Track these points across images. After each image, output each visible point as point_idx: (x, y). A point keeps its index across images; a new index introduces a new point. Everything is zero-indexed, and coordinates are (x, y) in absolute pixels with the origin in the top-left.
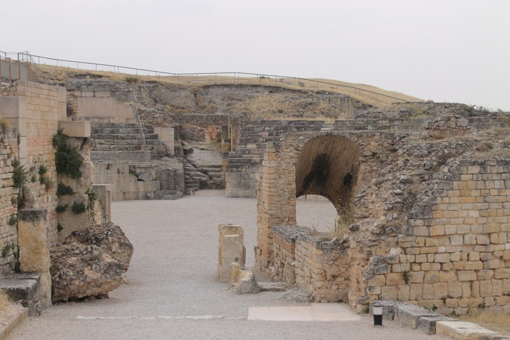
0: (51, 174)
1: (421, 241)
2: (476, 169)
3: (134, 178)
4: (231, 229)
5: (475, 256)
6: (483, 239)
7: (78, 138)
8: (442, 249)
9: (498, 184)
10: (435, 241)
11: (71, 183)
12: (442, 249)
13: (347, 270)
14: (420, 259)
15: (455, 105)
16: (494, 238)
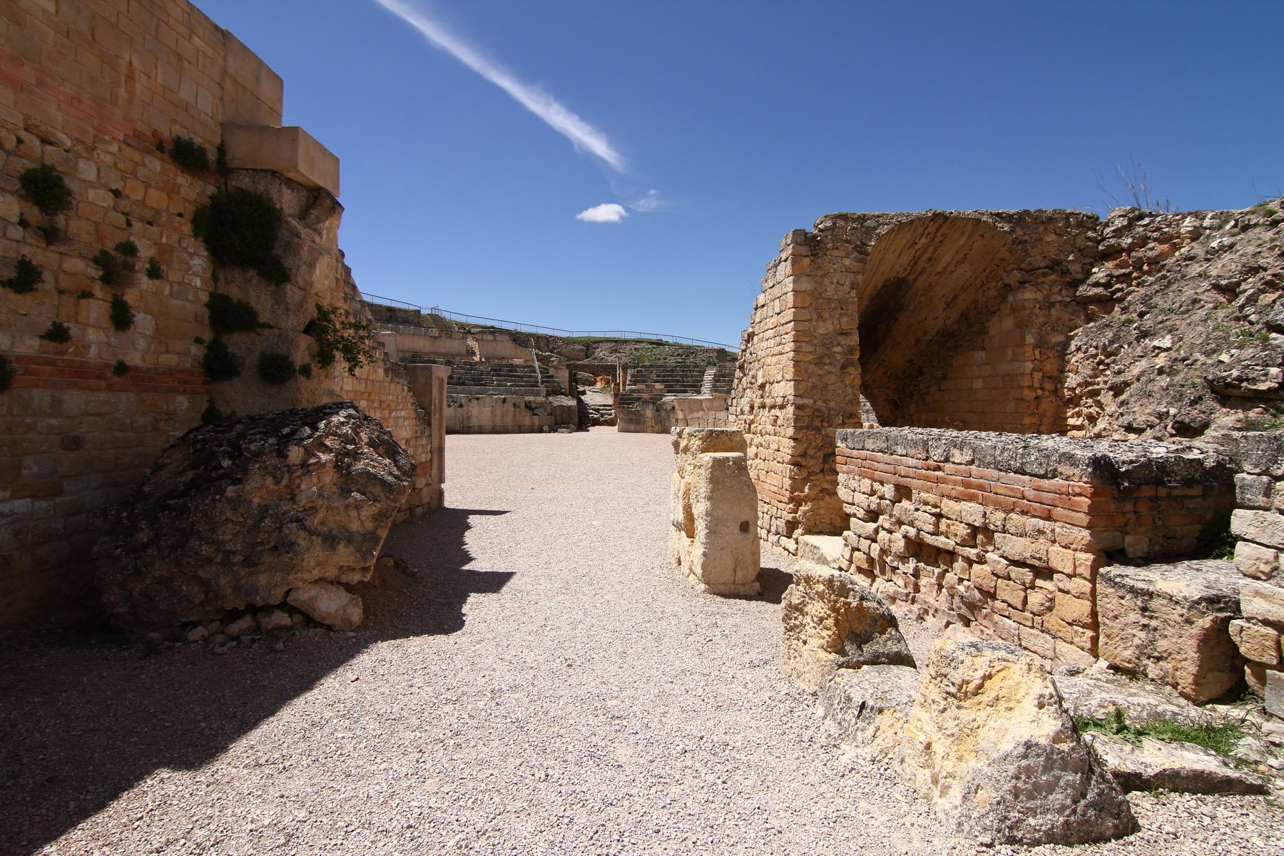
3: (529, 413)
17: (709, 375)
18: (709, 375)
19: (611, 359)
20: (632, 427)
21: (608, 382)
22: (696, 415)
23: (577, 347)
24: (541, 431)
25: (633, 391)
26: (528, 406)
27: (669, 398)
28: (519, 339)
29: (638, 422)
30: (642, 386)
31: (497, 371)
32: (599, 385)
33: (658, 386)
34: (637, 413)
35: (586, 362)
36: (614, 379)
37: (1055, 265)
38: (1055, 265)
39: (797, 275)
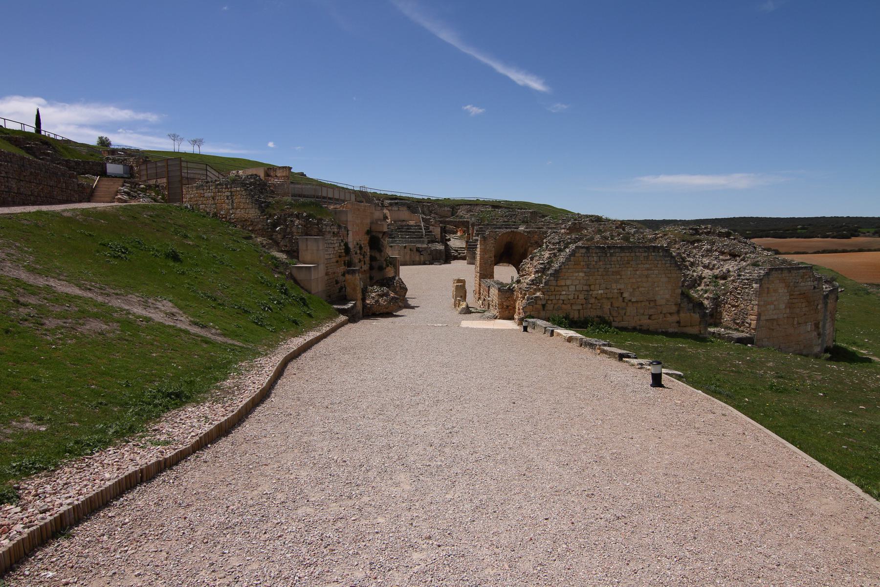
0: (367, 249)
1: (552, 288)
2: (584, 251)
3: (418, 254)
4: (459, 281)
5: (581, 296)
6: (585, 288)
7: (380, 232)
8: (564, 293)
9: (595, 259)
10: (560, 289)
11: (377, 255)
12: (564, 293)
13: (588, 266)
14: (552, 297)
15: (592, 216)
16: (592, 287)
21: (464, 232)
24: (425, 264)
26: (418, 250)
31: (400, 228)
32: (459, 234)
35: (451, 219)
37: (536, 242)
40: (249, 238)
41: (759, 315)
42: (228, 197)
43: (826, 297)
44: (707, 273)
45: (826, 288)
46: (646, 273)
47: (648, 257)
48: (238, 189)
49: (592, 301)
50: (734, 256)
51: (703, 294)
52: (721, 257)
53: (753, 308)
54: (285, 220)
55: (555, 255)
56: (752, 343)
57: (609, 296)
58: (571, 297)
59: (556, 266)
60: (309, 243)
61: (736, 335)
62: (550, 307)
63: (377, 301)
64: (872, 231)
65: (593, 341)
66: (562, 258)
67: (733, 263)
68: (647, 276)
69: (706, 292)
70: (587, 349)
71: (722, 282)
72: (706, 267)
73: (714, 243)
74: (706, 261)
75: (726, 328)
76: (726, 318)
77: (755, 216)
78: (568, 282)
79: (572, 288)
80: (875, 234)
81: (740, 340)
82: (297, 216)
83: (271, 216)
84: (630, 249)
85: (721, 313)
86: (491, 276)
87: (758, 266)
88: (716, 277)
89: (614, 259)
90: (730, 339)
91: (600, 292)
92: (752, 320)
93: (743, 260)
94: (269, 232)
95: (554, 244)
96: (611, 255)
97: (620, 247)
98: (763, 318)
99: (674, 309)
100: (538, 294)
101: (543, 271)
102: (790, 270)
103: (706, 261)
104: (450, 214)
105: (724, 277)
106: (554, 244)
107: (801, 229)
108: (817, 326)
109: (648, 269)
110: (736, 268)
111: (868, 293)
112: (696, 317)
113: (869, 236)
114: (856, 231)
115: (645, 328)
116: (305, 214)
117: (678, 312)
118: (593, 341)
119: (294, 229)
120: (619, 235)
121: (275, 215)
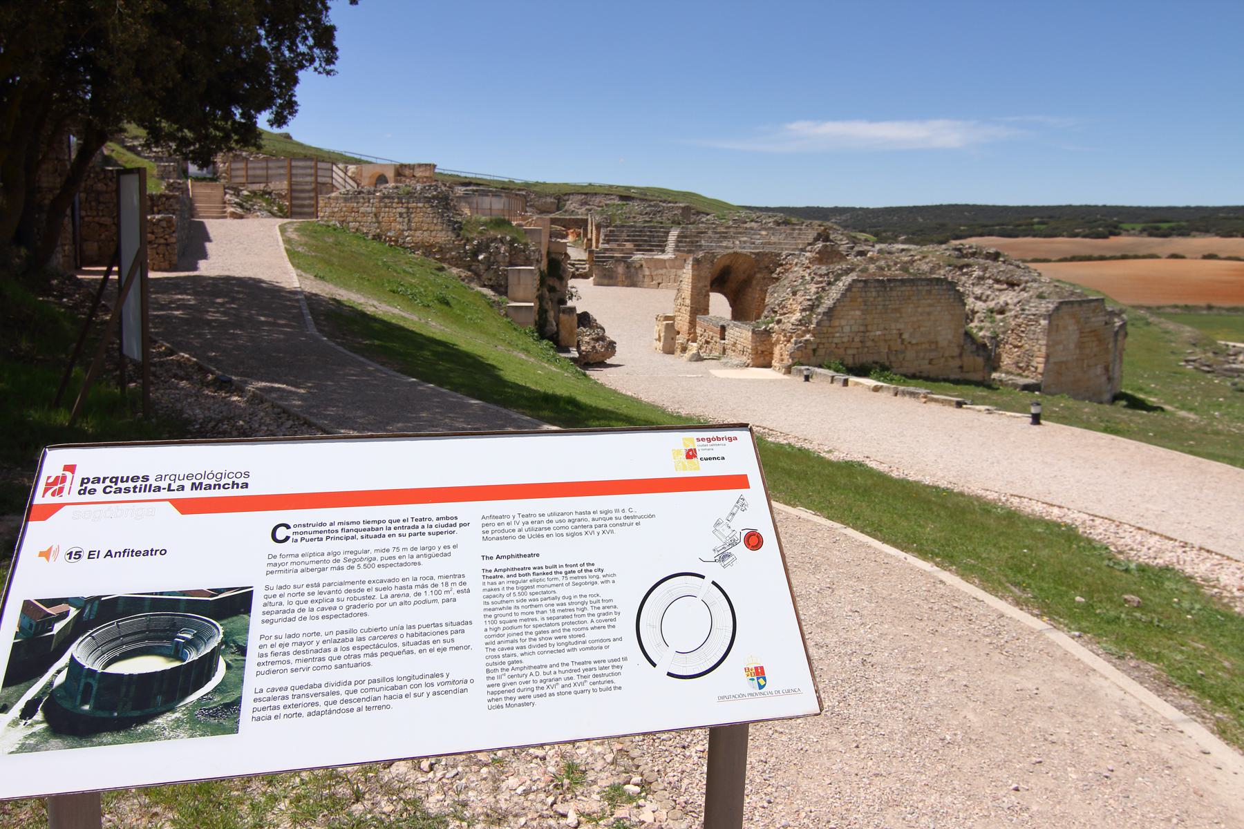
2: (861, 285)
5: (857, 339)
17: (674, 234)
18: (674, 234)
19: (581, 213)
20: (606, 281)
21: (578, 235)
22: (660, 272)
23: (549, 200)
25: (606, 250)
27: (638, 256)
28: (626, 196)
29: (611, 277)
30: (613, 245)
33: (629, 245)
34: (610, 270)
36: (585, 235)
37: (767, 267)
38: (767, 267)
39: (693, 269)
40: (441, 269)
41: (1047, 357)
42: (401, 215)
43: (1116, 333)
44: (979, 305)
45: (1118, 323)
46: (928, 309)
47: (929, 292)
48: (420, 205)
49: (869, 344)
50: (1012, 285)
51: (981, 330)
52: (996, 286)
53: (1039, 349)
54: (488, 247)
55: (823, 289)
56: (1039, 390)
57: (888, 337)
58: (845, 340)
59: (828, 303)
60: (522, 275)
61: (1022, 381)
62: (821, 352)
63: (594, 347)
64: (1139, 227)
65: (912, 389)
66: (835, 293)
67: (1012, 293)
68: (929, 314)
69: (981, 329)
70: (907, 398)
71: (999, 317)
72: (978, 298)
73: (986, 269)
74: (978, 291)
75: (1008, 373)
76: (1006, 361)
77: (971, 203)
78: (843, 322)
79: (847, 329)
80: (1142, 231)
81: (1026, 387)
82: (502, 241)
83: (468, 240)
84: (913, 282)
85: (1000, 355)
86: (705, 311)
87: (1044, 298)
88: (991, 311)
89: (894, 293)
90: (1015, 386)
91: (878, 333)
92: (1039, 363)
93: (1024, 290)
94: (467, 261)
95: (821, 276)
96: (891, 289)
97: (902, 280)
98: (1052, 360)
99: (956, 351)
100: (808, 336)
101: (812, 308)
102: (1081, 303)
103: (978, 291)
104: (554, 207)
105: (1002, 312)
106: (821, 276)
107: (1039, 223)
108: (1107, 369)
109: (930, 305)
110: (1016, 300)
111: (1148, 324)
112: (980, 361)
113: (1134, 235)
114: (1116, 227)
115: (924, 375)
116: (508, 238)
117: (961, 355)
118: (912, 389)
119: (500, 258)
120: (896, 264)
121: (474, 239)
